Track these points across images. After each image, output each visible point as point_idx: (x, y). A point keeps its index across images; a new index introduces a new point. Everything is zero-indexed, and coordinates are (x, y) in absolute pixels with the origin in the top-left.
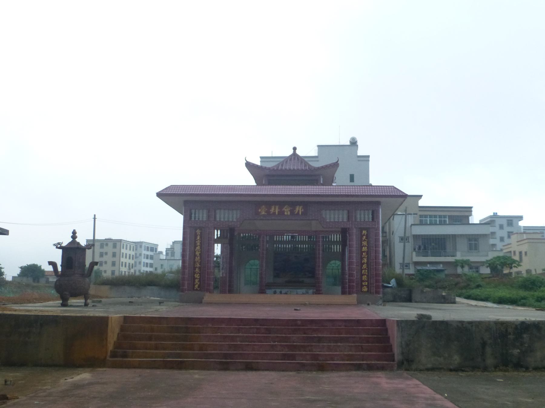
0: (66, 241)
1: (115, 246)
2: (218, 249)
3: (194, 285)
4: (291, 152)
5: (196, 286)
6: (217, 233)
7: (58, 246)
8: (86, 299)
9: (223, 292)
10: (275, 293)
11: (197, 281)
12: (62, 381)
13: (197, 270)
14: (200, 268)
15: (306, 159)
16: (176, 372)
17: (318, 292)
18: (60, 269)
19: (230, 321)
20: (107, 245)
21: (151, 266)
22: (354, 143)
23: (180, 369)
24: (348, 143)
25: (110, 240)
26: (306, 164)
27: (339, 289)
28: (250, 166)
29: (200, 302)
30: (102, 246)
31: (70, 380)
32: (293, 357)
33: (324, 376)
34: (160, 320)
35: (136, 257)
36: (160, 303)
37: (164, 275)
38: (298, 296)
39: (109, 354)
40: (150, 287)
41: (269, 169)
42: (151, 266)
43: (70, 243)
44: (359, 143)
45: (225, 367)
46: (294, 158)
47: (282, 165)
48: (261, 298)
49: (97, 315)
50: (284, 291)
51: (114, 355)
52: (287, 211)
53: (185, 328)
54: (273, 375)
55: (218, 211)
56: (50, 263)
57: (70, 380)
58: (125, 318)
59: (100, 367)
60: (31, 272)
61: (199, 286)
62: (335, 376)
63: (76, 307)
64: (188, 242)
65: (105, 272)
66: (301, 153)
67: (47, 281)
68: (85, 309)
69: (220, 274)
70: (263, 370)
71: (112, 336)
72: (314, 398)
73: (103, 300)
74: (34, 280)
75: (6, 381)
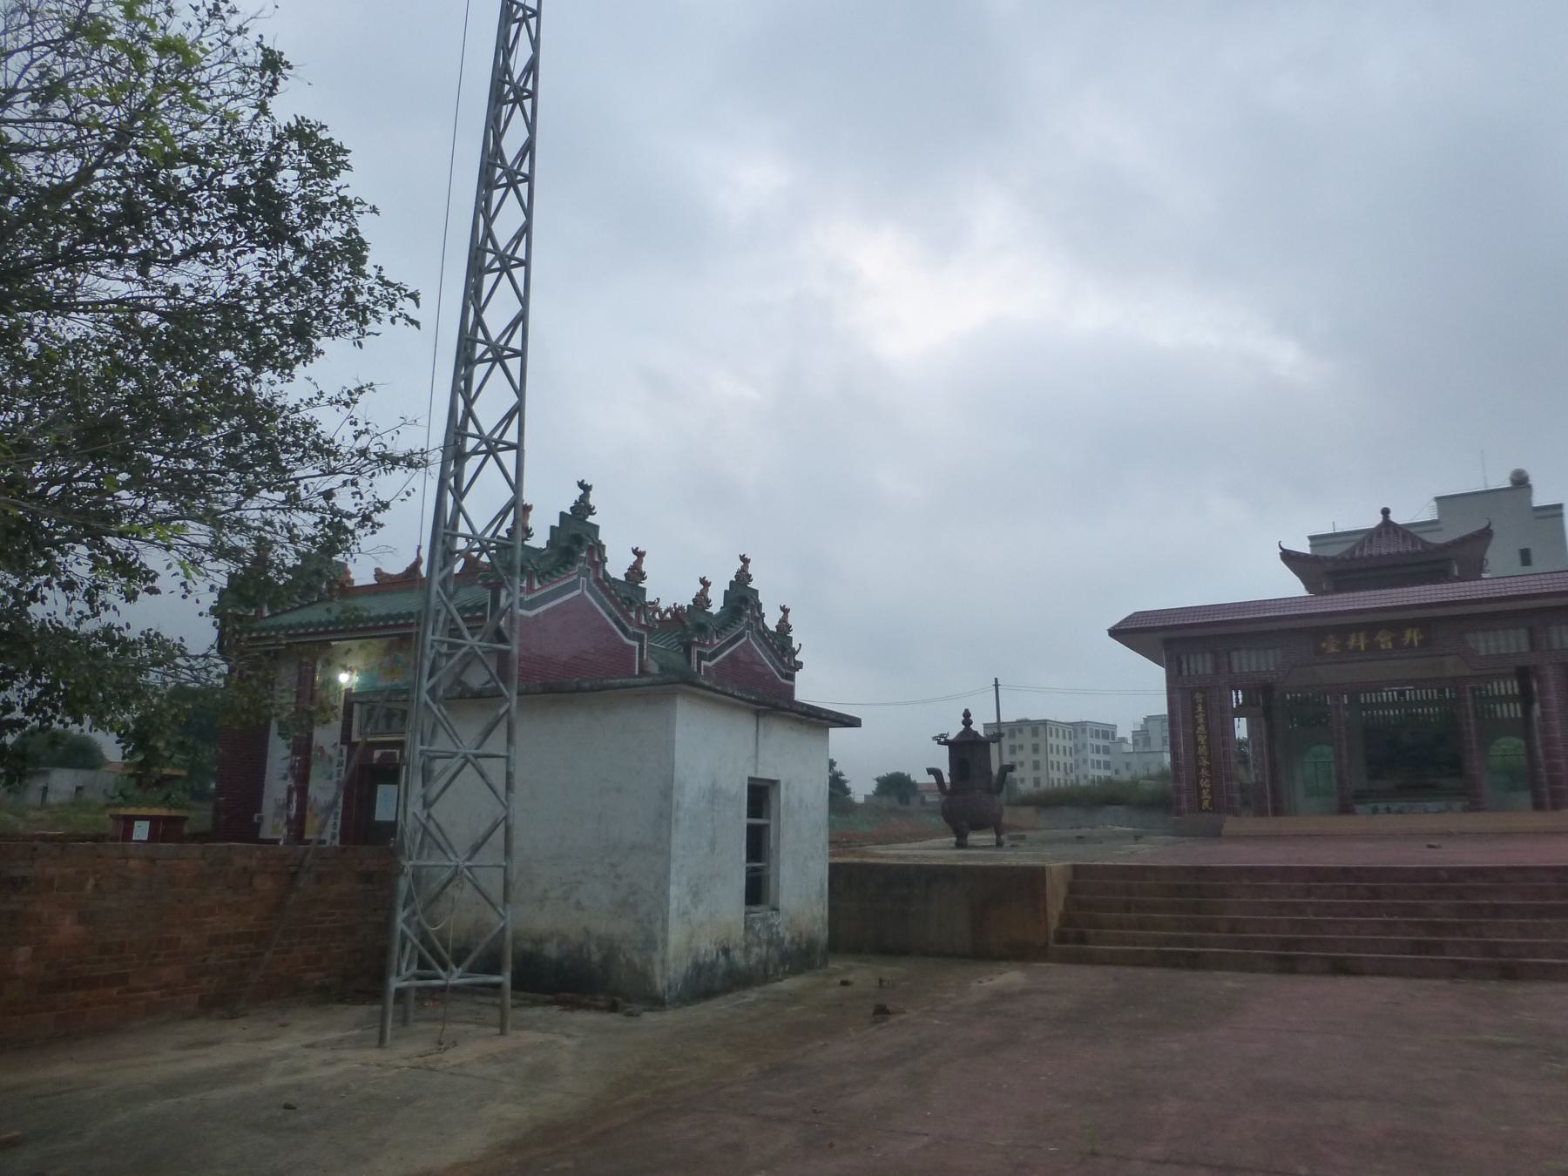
0: (955, 729)
1: (1035, 733)
2: (1241, 728)
3: (1200, 802)
4: (1379, 519)
5: (1206, 804)
6: (1238, 697)
7: (941, 740)
8: (998, 834)
9: (1261, 812)
10: (1375, 811)
11: (1205, 792)
12: (974, 984)
13: (1204, 772)
14: (1209, 768)
15: (1412, 530)
16: (1186, 974)
17: (1475, 806)
18: (947, 780)
19: (1286, 872)
20: (1021, 731)
21: (1107, 766)
22: (1521, 482)
23: (1194, 967)
24: (1508, 484)
25: (1025, 722)
26: (1415, 539)
27: (1525, 798)
28: (1289, 557)
29: (1216, 834)
30: (1012, 735)
31: (986, 984)
32: (1439, 948)
33: (1518, 991)
34: (1141, 871)
35: (1077, 751)
36: (1137, 838)
37: (1134, 782)
38: (1429, 817)
39: (1052, 935)
40: (1112, 808)
41: (1333, 559)
42: (1107, 766)
43: (961, 734)
44: (1533, 481)
45: (1287, 965)
46: (1387, 533)
47: (1362, 549)
48: (1345, 823)
49: (1023, 863)
50: (1395, 806)
51: (1062, 938)
52: (1385, 640)
53: (1194, 890)
54: (1395, 987)
55: (1235, 654)
56: (931, 771)
57: (986, 984)
58: (1075, 867)
59: (1038, 961)
60: (895, 786)
61: (1211, 804)
62: (1544, 991)
63: (982, 850)
64: (1179, 718)
65: (1022, 780)
66: (1398, 518)
67: (923, 802)
68: (1000, 853)
69: (1250, 776)
70: (1372, 974)
71: (1055, 906)
72: (1504, 1039)
73: (1028, 834)
74: (901, 802)
75: (881, 981)
